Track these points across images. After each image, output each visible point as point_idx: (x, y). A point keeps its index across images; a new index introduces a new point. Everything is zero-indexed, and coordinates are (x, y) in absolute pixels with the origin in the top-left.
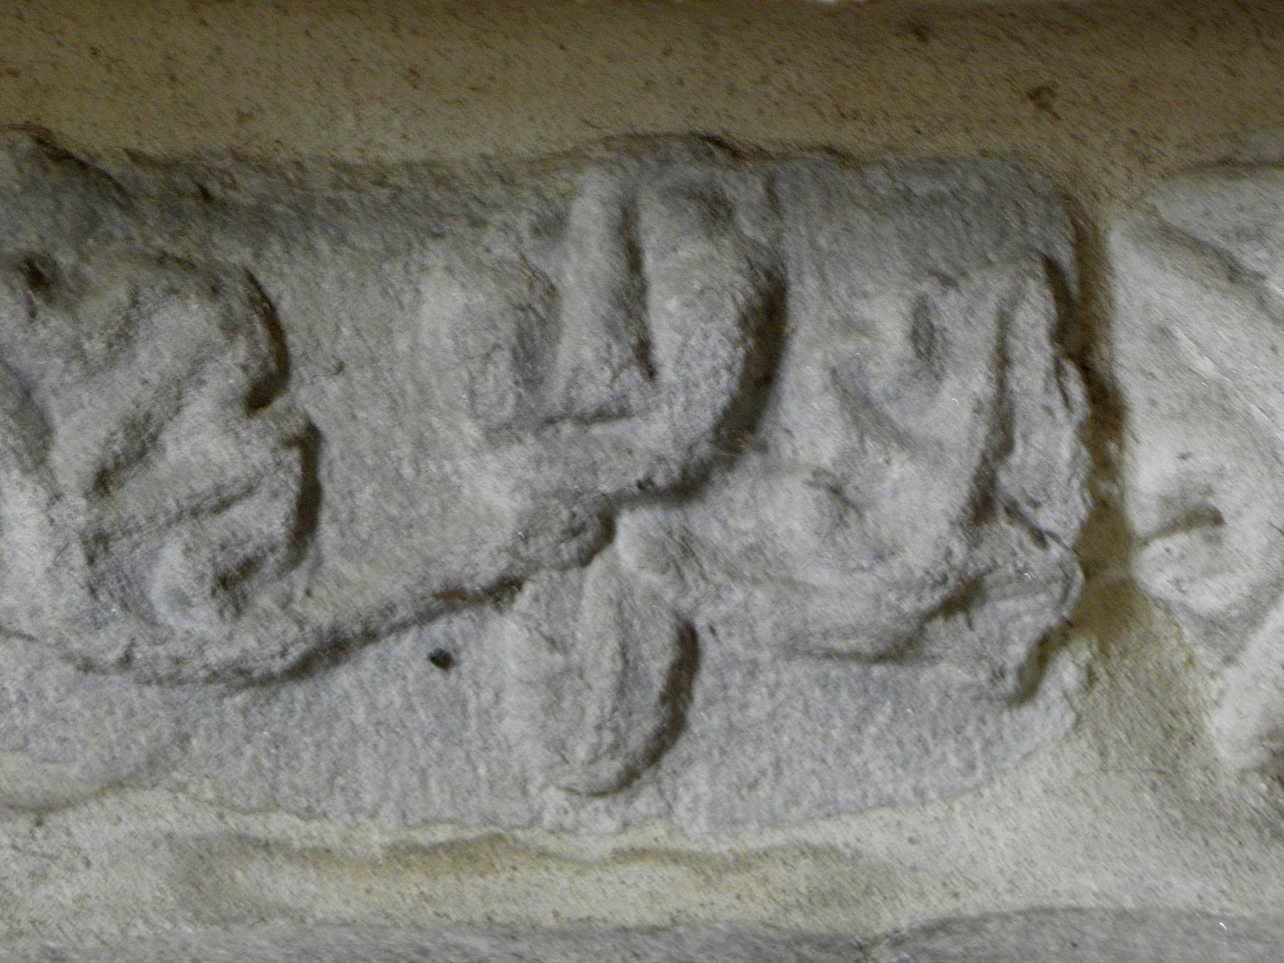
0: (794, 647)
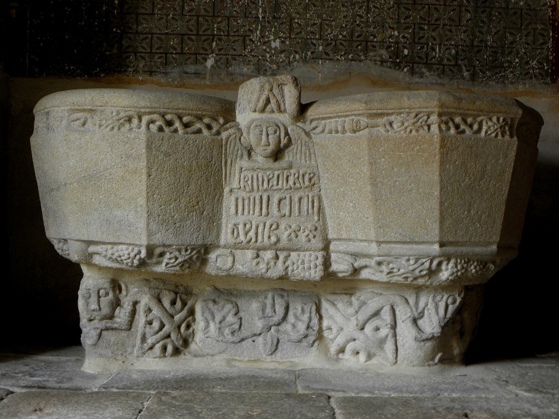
0: (289, 341)
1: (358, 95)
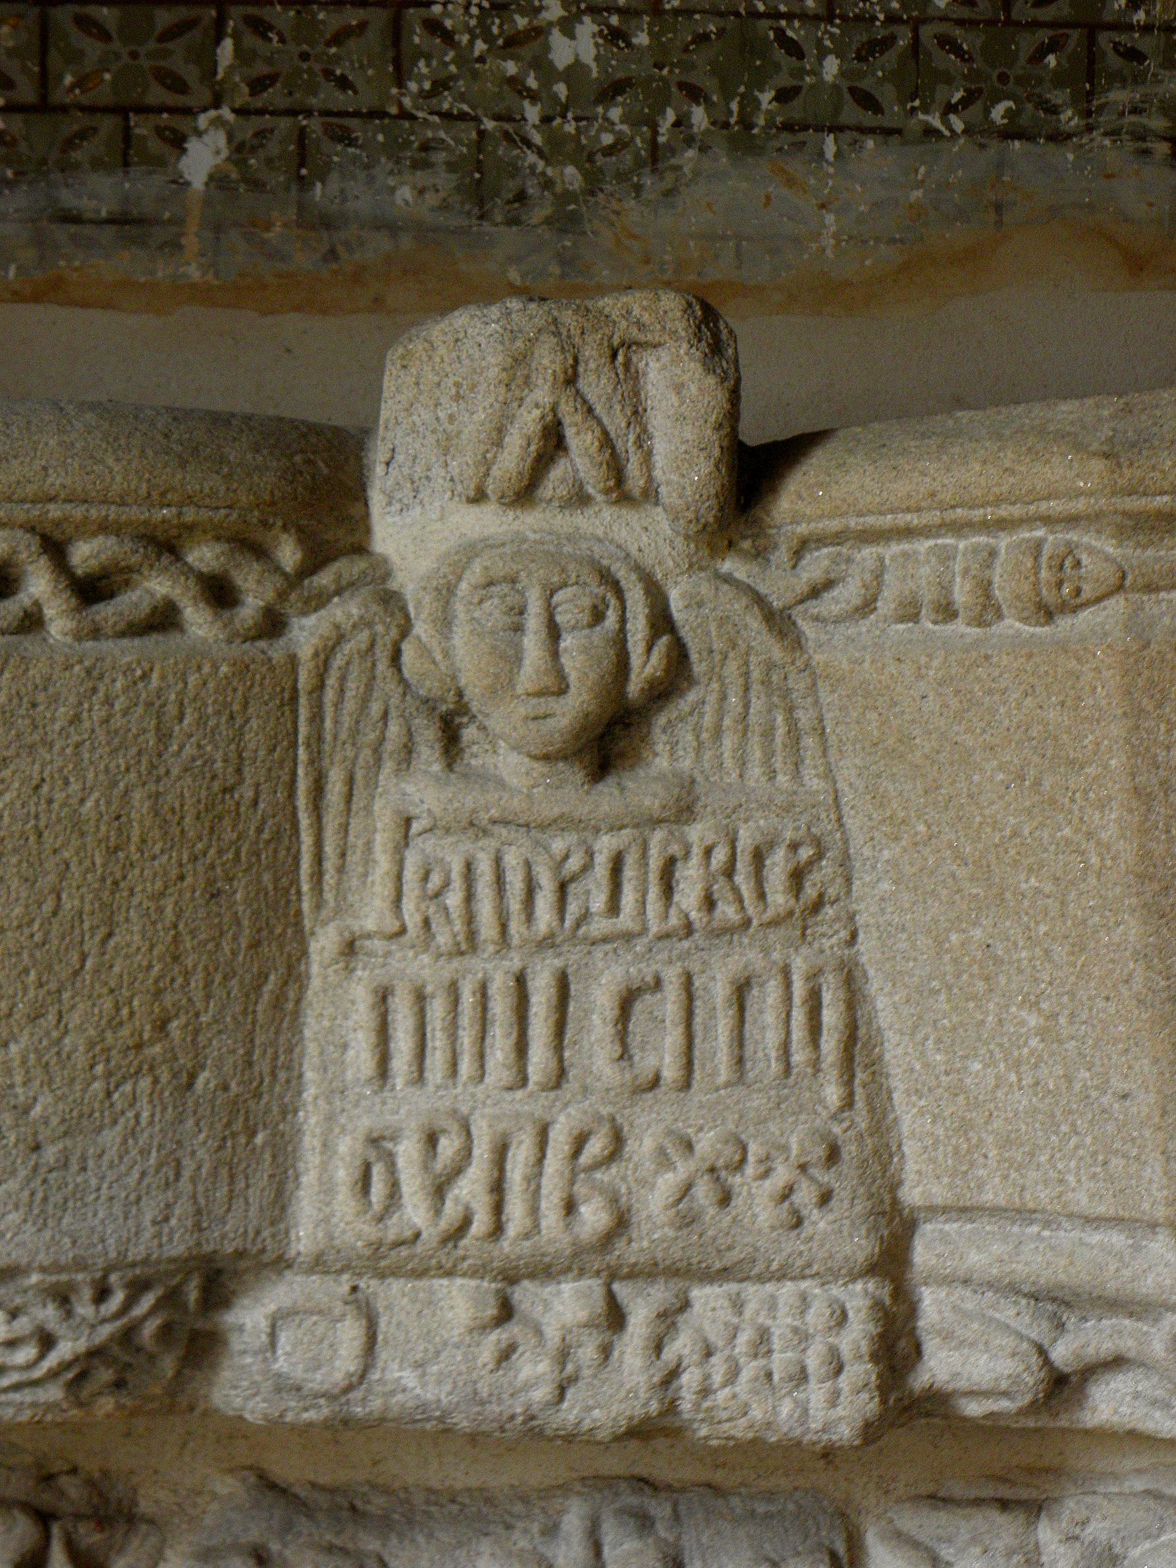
1: (1064, 407)
